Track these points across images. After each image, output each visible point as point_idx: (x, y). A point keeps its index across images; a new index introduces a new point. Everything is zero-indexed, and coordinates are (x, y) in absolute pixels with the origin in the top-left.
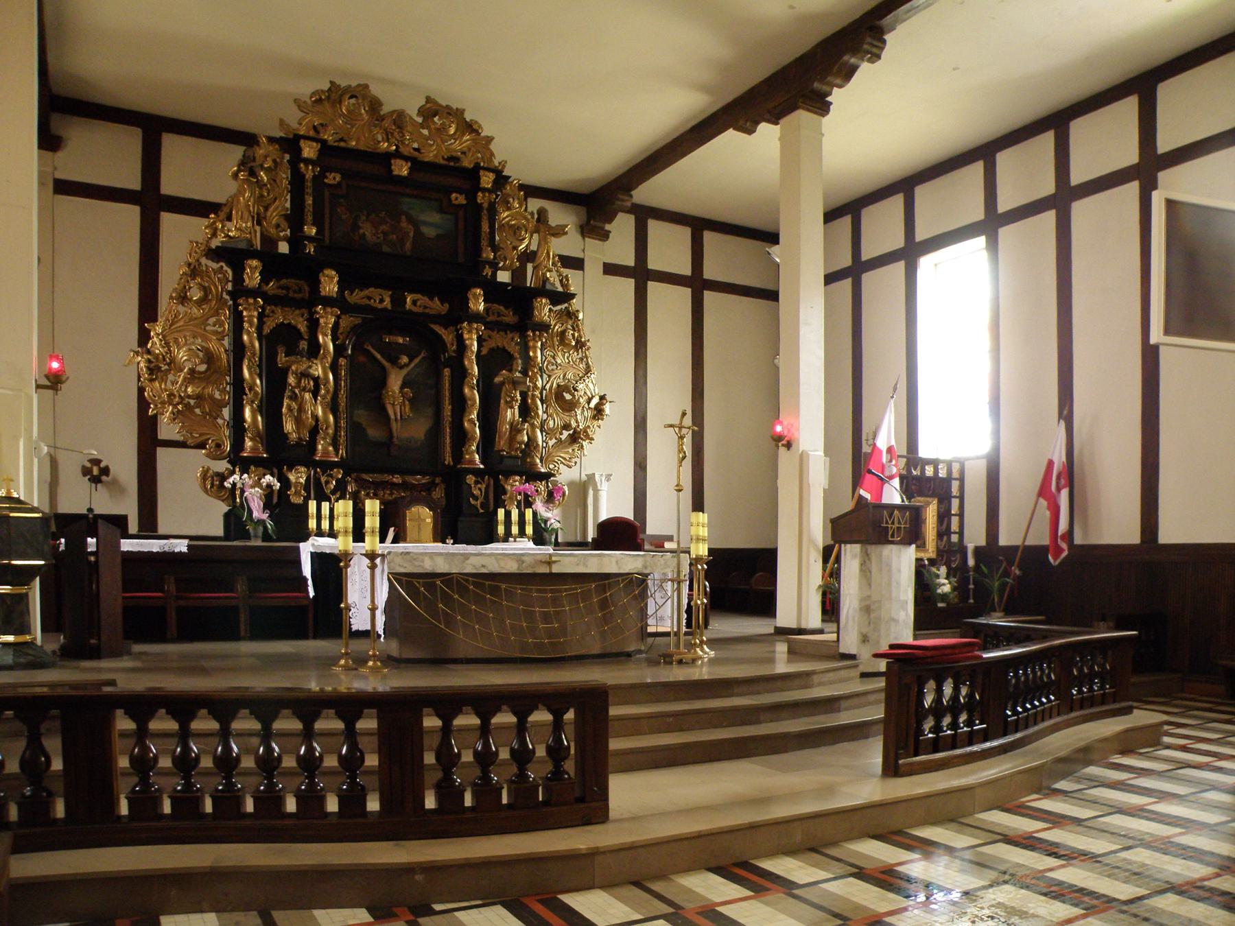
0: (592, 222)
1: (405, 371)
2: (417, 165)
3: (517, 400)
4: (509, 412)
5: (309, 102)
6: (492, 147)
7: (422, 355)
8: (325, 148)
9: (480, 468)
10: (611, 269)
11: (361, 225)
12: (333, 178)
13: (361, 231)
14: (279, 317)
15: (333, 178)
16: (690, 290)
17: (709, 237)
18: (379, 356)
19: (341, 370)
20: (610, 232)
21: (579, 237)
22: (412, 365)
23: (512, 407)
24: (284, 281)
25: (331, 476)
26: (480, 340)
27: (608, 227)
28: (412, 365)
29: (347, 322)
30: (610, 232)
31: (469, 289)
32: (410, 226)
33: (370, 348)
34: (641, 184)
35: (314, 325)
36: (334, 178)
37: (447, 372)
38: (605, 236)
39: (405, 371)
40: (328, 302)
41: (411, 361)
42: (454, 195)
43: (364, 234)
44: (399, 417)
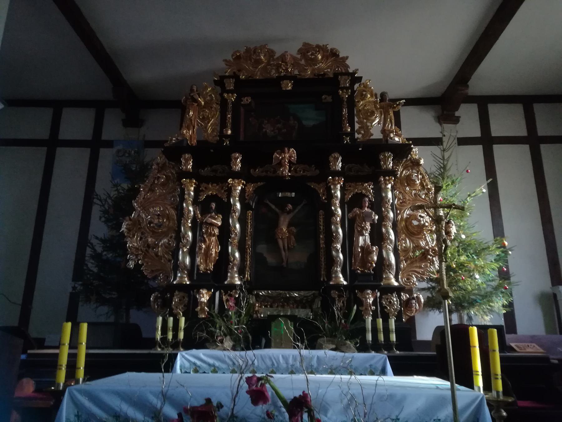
0: (445, 112)
1: (291, 215)
2: (298, 81)
3: (367, 230)
4: (361, 238)
5: (232, 60)
6: (348, 62)
7: (304, 203)
8: (239, 84)
9: (186, 284)
10: (463, 141)
11: (264, 126)
12: (247, 100)
13: (264, 130)
14: (212, 190)
15: (247, 100)
16: (528, 146)
17: (538, 108)
18: (273, 207)
19: (323, 229)
20: (460, 117)
21: (438, 125)
22: (297, 210)
23: (363, 235)
24: (214, 167)
25: (231, 296)
26: (342, 189)
27: (457, 114)
28: (297, 210)
29: (251, 188)
30: (460, 117)
31: (330, 154)
32: (296, 122)
33: (268, 202)
34: (473, 74)
35: (229, 191)
36: (247, 100)
37: (321, 212)
38: (456, 120)
39: (291, 215)
40: (236, 176)
41: (294, 208)
42: (323, 97)
43: (266, 131)
44: (286, 247)
